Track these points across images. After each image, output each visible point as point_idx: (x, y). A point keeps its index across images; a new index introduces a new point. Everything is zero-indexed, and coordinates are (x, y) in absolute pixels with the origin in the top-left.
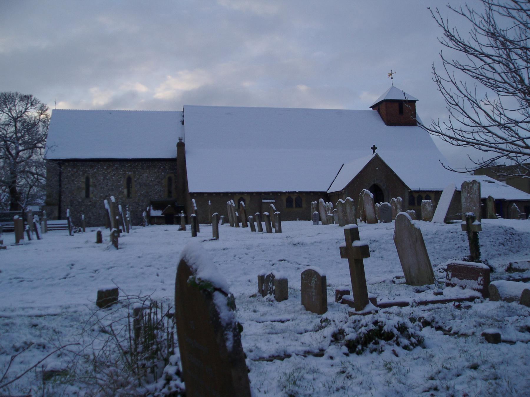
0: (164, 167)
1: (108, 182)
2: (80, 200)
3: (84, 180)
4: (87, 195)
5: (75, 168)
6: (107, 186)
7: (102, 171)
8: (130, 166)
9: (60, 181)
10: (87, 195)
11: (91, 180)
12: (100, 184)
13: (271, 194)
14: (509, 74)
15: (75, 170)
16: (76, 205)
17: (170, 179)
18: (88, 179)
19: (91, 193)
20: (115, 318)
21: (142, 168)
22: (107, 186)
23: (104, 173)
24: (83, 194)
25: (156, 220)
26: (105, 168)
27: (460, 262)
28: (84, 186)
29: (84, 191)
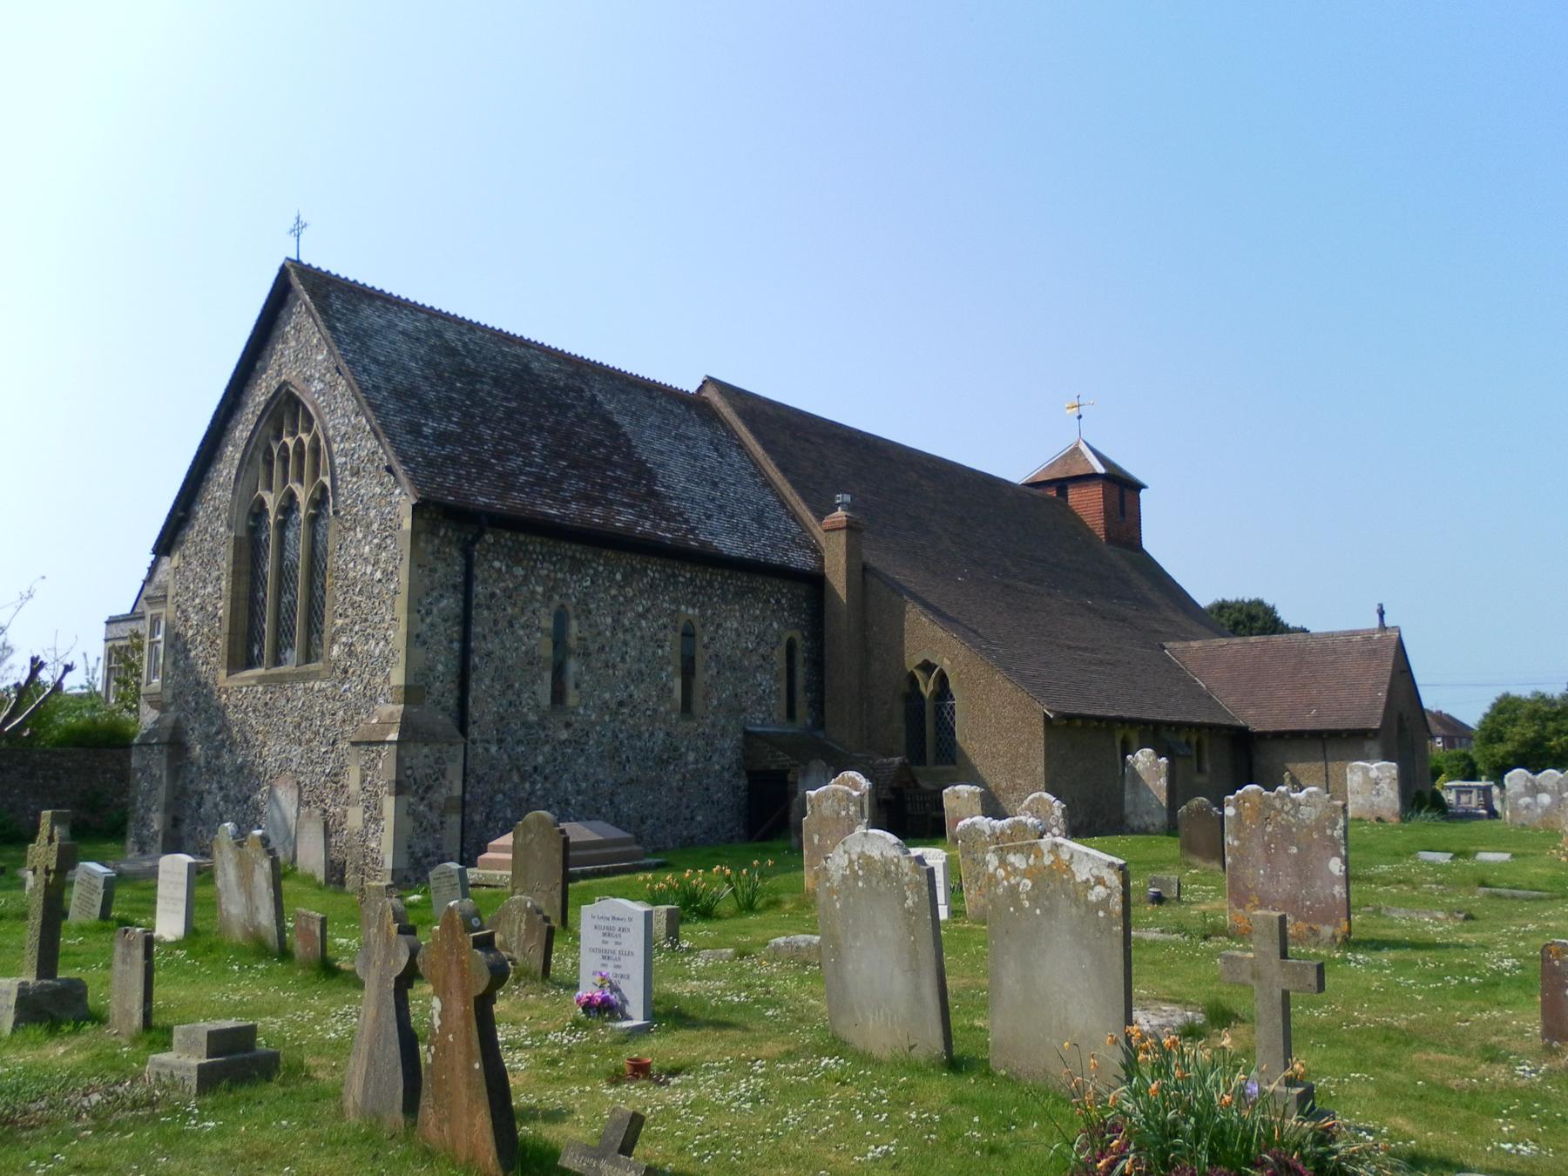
0: (778, 601)
1: (625, 643)
2: (532, 717)
3: (548, 623)
4: (558, 695)
5: (518, 562)
6: (623, 660)
7: (606, 591)
8: (692, 580)
9: (466, 620)
10: (558, 695)
11: (574, 627)
12: (602, 649)
13: (1079, 723)
14: (1436, 1076)
15: (519, 571)
16: (519, 742)
17: (791, 647)
18: (561, 619)
19: (570, 684)
20: (685, 1086)
21: (724, 599)
22: (623, 660)
23: (614, 597)
24: (544, 691)
25: (1511, 761)
26: (618, 577)
27: (205, 1061)
28: (546, 650)
29: (548, 676)
